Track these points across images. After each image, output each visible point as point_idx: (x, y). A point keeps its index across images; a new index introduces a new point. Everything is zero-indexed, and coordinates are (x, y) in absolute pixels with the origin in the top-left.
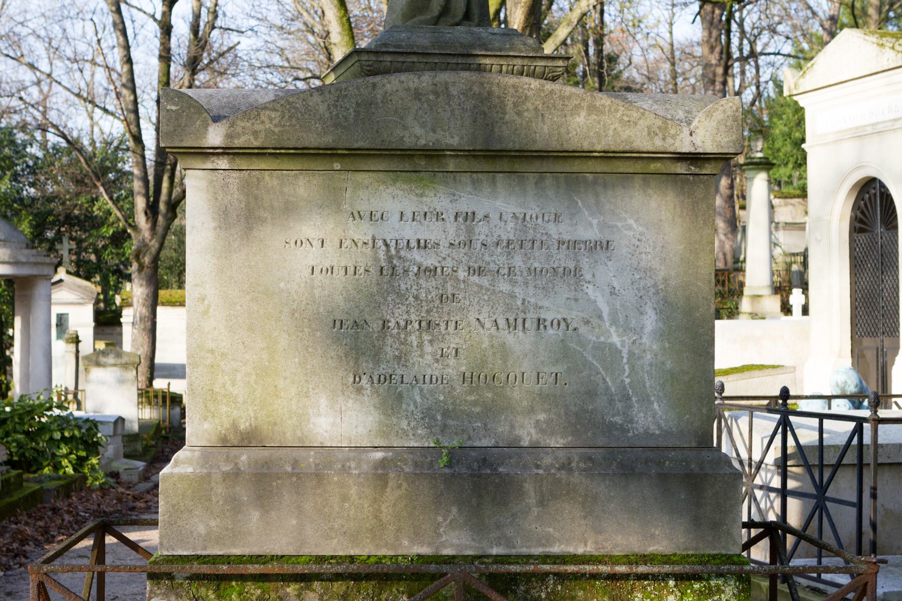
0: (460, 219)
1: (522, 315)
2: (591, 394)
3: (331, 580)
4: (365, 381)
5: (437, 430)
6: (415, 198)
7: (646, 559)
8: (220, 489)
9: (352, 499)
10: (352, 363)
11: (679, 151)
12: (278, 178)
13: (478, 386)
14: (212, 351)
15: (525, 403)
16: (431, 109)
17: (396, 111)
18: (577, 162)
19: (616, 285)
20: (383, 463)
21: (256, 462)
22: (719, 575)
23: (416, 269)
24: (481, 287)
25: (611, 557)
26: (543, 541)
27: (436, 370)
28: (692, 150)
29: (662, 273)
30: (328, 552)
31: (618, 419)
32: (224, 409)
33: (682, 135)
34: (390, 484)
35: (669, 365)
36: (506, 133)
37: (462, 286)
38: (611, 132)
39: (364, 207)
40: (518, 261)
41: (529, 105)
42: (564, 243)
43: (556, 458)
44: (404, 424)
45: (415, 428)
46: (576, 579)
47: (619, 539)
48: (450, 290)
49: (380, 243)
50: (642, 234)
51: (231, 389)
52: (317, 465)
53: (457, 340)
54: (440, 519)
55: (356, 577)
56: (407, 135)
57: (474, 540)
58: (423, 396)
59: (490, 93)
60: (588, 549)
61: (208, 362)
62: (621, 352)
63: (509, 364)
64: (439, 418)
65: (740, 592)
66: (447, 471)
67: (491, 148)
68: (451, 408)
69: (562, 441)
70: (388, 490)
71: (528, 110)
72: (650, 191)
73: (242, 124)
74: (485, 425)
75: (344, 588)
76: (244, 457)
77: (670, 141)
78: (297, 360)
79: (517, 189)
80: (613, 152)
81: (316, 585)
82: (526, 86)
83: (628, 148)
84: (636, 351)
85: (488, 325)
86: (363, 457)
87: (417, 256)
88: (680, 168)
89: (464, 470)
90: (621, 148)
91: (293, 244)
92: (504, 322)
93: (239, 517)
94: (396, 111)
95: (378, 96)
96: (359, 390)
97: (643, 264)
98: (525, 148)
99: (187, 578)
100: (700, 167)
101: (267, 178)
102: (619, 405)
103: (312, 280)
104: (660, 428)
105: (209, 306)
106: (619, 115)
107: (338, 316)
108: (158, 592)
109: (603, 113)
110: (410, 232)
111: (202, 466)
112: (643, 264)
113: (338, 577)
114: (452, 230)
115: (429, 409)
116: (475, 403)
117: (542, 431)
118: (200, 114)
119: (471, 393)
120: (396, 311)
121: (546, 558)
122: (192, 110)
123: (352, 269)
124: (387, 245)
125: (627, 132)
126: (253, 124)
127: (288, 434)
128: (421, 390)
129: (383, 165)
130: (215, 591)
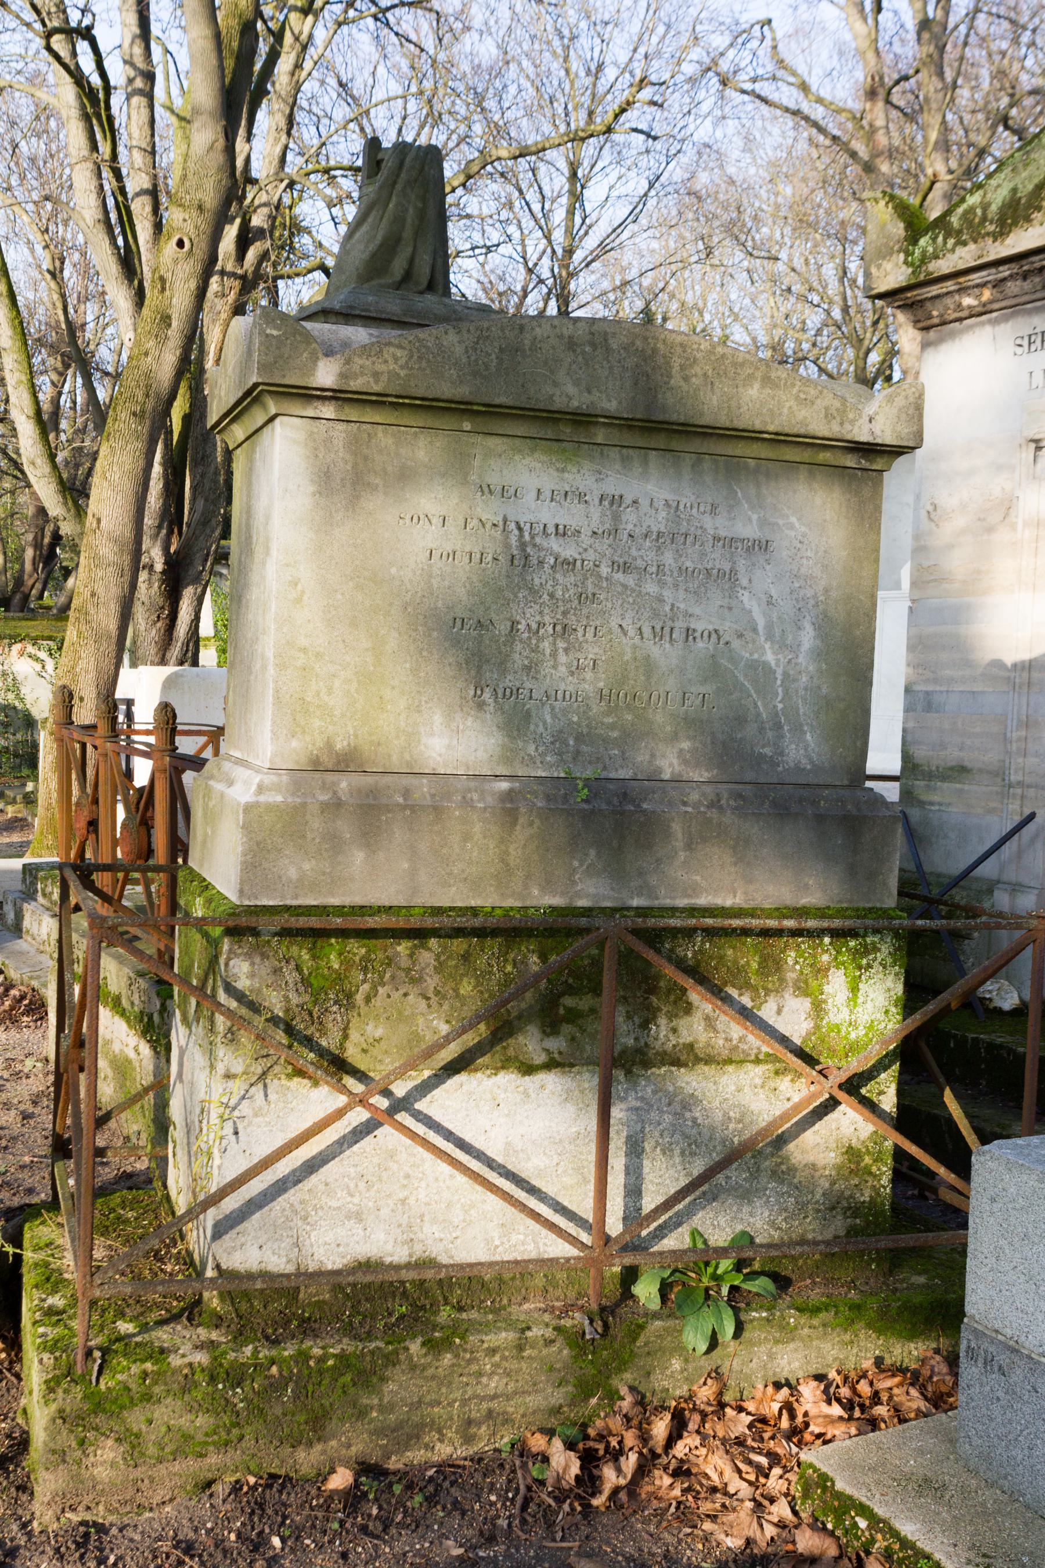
0: (606, 503)
1: (669, 624)
2: (741, 720)
3: (450, 937)
4: (487, 695)
5: (568, 757)
6: (556, 474)
7: (801, 912)
8: (316, 823)
9: (476, 838)
10: (473, 673)
11: (857, 439)
12: (393, 435)
13: (617, 706)
14: (304, 650)
15: (668, 728)
16: (587, 364)
17: (546, 363)
18: (741, 444)
19: (773, 593)
20: (509, 796)
21: (359, 791)
22: (876, 931)
23: (552, 561)
24: (625, 586)
25: (762, 910)
26: (689, 892)
27: (570, 685)
28: (870, 439)
29: (823, 583)
30: (446, 903)
31: (768, 751)
32: (317, 723)
33: (861, 421)
34: (521, 821)
35: (825, 690)
36: (671, 401)
37: (605, 584)
38: (785, 411)
39: (494, 479)
40: (668, 558)
41: (697, 369)
42: (719, 540)
43: (704, 794)
44: (531, 749)
45: (543, 755)
46: (726, 935)
47: (771, 889)
48: (590, 589)
49: (512, 526)
50: (804, 535)
51: (326, 699)
52: (433, 796)
53: (596, 650)
54: (576, 863)
55: (480, 933)
56: (558, 393)
57: (612, 889)
58: (554, 716)
59: (655, 351)
60: (737, 901)
61: (300, 663)
62: (775, 672)
63: (653, 680)
64: (571, 743)
65: (896, 950)
66: (586, 806)
67: (653, 418)
68: (585, 732)
69: (706, 774)
70: (518, 827)
71: (696, 375)
72: (815, 485)
73: (361, 362)
74: (623, 753)
75: (465, 946)
76: (344, 784)
77: (848, 426)
78: (408, 666)
79: (671, 471)
80: (787, 435)
81: (433, 942)
82: (695, 346)
83: (802, 431)
84: (792, 672)
85: (631, 632)
86: (487, 786)
87: (554, 544)
88: (850, 461)
89: (604, 806)
90: (795, 431)
91: (408, 521)
92: (650, 630)
93: (340, 858)
94: (546, 363)
95: (526, 342)
96: (481, 706)
97: (803, 570)
98: (691, 421)
99: (276, 934)
100: (871, 462)
101: (380, 435)
102: (770, 734)
103: (430, 566)
104: (812, 762)
105: (303, 592)
106: (795, 391)
107: (460, 613)
108: (239, 951)
109: (778, 386)
110: (547, 514)
111: (293, 794)
112: (803, 570)
113: (459, 932)
114: (595, 517)
115: (561, 732)
116: (612, 727)
117: (685, 762)
118: (308, 343)
119: (608, 714)
120: (528, 611)
121: (693, 911)
122: (298, 338)
123: (478, 556)
124: (520, 529)
125: (803, 412)
126: (374, 363)
127: (394, 758)
128: (553, 708)
129: (521, 429)
130: (310, 950)
